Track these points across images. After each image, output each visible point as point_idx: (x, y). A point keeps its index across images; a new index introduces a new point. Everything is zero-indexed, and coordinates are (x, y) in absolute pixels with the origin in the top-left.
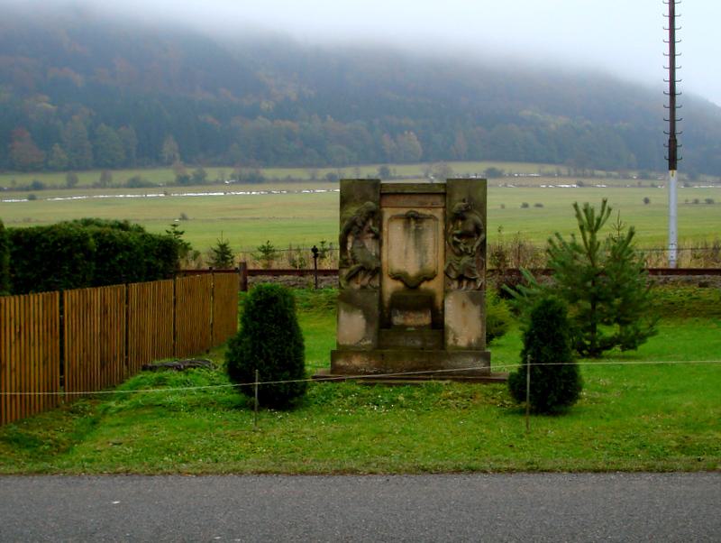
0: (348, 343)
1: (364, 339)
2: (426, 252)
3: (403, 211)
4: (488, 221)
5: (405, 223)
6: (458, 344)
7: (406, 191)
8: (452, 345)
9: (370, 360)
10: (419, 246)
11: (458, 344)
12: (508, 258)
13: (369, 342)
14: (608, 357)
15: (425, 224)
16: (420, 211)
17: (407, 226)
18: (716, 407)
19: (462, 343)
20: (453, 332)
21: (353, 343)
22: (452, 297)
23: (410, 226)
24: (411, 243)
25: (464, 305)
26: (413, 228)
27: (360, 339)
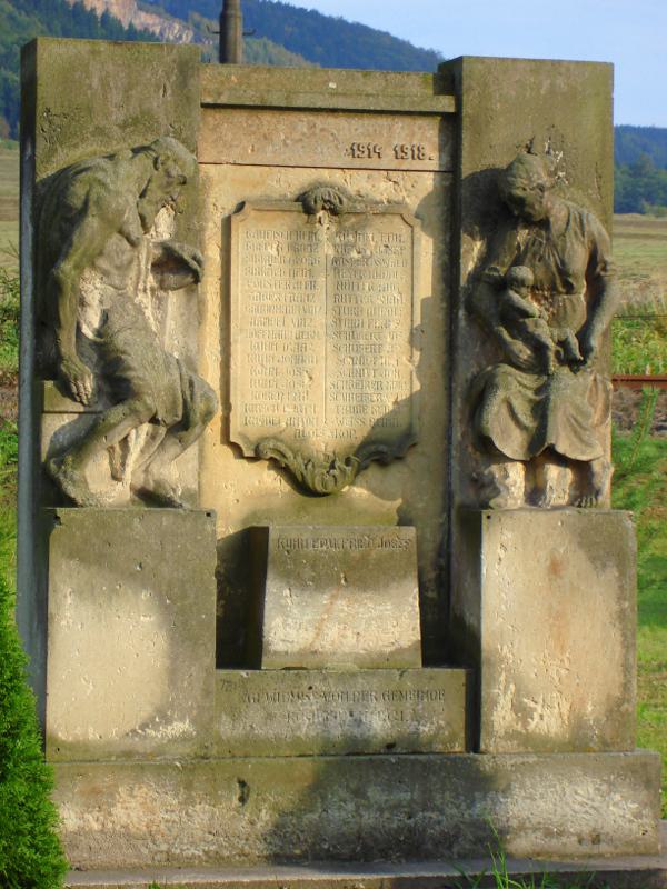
0: (93, 735)
1: (163, 716)
2: (376, 349)
3: (292, 182)
4: (464, 103)
5: (298, 233)
6: (534, 724)
7: (299, 103)
8: (510, 735)
9: (189, 801)
10: (349, 326)
11: (534, 724)
12: (157, 31)
13: (180, 727)
14: (313, 484)
15: (372, 239)
16: (356, 184)
17: (300, 245)
18: (645, 847)
19: (549, 721)
20: (518, 681)
21: (113, 733)
22: (508, 536)
23: (313, 244)
24: (320, 318)
25: (555, 568)
26: (327, 251)
27: (146, 710)
